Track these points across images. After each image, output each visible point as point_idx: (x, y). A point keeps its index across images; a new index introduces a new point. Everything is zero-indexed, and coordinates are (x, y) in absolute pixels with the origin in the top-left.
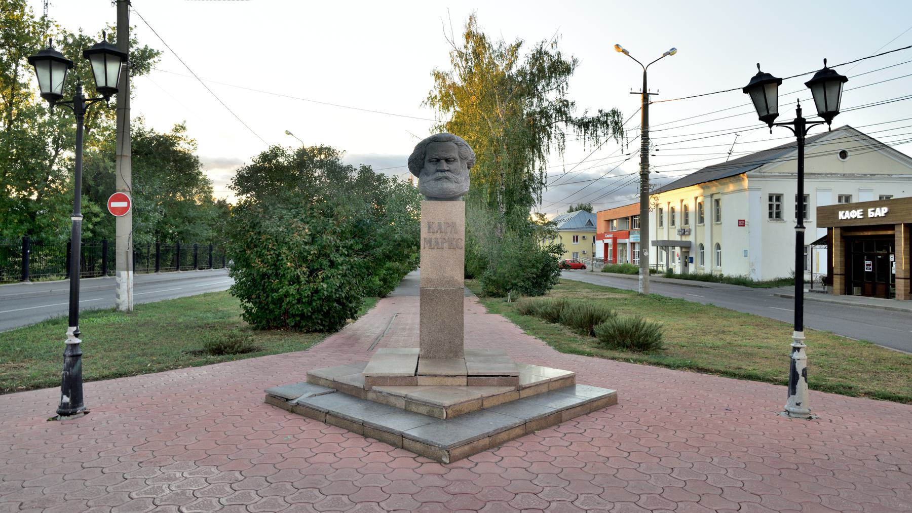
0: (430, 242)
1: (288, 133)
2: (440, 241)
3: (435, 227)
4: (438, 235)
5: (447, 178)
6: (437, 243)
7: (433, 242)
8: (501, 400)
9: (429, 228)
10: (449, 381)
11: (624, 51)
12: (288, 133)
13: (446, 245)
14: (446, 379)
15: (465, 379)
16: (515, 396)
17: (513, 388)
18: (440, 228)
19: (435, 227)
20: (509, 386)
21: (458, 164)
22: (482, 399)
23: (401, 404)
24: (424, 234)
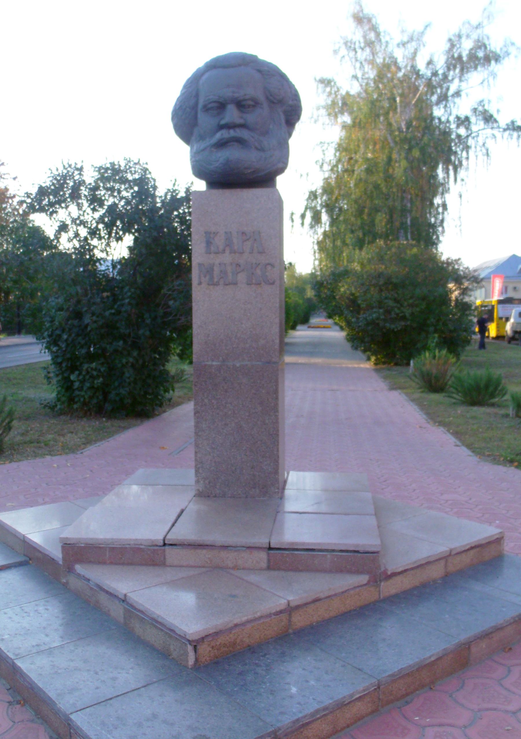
0: (209, 271)
1: (307, 175)
2: (229, 269)
3: (219, 242)
4: (227, 258)
5: (240, 141)
6: (224, 273)
7: (217, 271)
8: (337, 607)
9: (209, 243)
10: (229, 558)
11: (476, 163)
12: (307, 175)
13: (242, 277)
14: (223, 554)
15: (263, 555)
16: (369, 595)
17: (364, 579)
18: (229, 243)
19: (219, 242)
20: (358, 572)
21: (264, 111)
22: (290, 610)
23: (117, 611)
24: (199, 255)
